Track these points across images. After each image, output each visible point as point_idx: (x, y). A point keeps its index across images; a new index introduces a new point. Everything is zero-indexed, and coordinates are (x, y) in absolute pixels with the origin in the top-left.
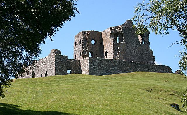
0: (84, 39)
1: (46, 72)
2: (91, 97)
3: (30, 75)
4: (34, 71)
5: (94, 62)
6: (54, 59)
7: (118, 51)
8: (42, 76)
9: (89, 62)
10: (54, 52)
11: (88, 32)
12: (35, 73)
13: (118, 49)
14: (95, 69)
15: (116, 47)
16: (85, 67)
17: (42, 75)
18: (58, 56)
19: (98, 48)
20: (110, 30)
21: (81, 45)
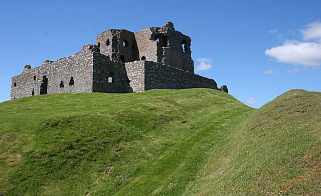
0: (115, 39)
1: (72, 78)
2: (108, 139)
3: (39, 81)
4: (46, 76)
5: (150, 68)
6: (89, 58)
7: (163, 56)
8: (33, 93)
9: (145, 68)
10: (90, 49)
11: (118, 30)
12: (47, 79)
13: (163, 54)
14: (152, 79)
15: (159, 52)
16: (136, 75)
17: (62, 82)
18: (97, 55)
19: (130, 52)
20: (151, 30)
21: (110, 47)
